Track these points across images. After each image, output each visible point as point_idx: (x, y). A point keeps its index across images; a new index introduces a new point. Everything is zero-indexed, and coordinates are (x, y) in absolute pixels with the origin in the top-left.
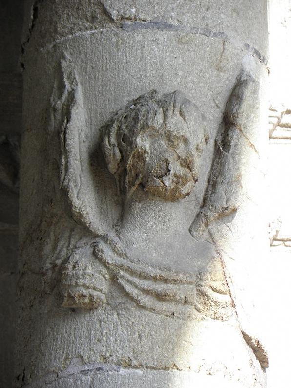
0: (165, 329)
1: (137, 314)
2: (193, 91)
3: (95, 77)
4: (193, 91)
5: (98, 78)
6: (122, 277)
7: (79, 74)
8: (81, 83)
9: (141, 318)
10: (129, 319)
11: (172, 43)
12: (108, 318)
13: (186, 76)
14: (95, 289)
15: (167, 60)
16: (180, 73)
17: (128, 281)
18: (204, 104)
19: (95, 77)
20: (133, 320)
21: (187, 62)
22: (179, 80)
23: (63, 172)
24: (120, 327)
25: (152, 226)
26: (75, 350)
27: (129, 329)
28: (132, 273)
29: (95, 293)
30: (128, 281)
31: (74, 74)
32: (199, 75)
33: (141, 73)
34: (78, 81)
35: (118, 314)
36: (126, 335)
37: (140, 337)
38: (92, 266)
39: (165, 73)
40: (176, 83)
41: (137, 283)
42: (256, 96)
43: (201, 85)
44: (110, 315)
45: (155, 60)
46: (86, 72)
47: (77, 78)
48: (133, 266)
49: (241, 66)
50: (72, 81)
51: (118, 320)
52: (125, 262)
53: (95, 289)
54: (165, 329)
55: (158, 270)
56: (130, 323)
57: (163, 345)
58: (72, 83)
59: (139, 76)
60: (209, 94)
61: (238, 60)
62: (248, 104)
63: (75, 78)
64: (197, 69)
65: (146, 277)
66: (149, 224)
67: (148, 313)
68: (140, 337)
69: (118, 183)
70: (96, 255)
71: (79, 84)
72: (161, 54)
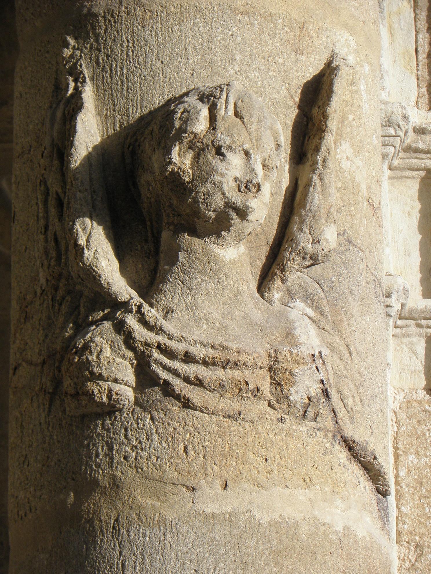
0: (222, 437)
1: (181, 415)
2: (259, 84)
3: (111, 70)
4: (259, 84)
5: (116, 71)
6: (156, 361)
7: (88, 67)
8: (92, 79)
9: (188, 422)
10: (169, 424)
11: (226, 13)
12: (138, 424)
13: (248, 62)
14: (116, 381)
15: (219, 38)
16: (239, 57)
17: (165, 367)
18: (277, 103)
19: (111, 70)
20: (176, 425)
21: (249, 40)
22: (237, 68)
23: (41, 215)
24: (156, 438)
25: (200, 284)
26: (122, 69)
27: (170, 439)
28: (171, 354)
29: (116, 387)
30: (165, 367)
31: (81, 66)
32: (268, 60)
33: (179, 59)
34: (86, 76)
35: (152, 419)
36: (165, 448)
37: (186, 450)
38: (111, 348)
39: (216, 58)
40: (232, 72)
41: (179, 370)
42: (355, 88)
43: (271, 74)
44: (141, 420)
45: (200, 40)
46: (98, 63)
47: (86, 71)
48: (172, 344)
49: (331, 45)
50: (78, 77)
51: (152, 427)
52: (161, 339)
53: (116, 381)
54: (222, 437)
55: (210, 349)
56: (171, 429)
57: (221, 462)
58: (76, 81)
59: (176, 63)
60: (283, 88)
61: (327, 37)
62: (344, 100)
63: (81, 72)
64: (263, 52)
65: (188, 358)
66: (195, 281)
67: (197, 413)
68: (186, 450)
69: (148, 223)
70: (120, 327)
71: (88, 80)
72: (209, 31)
